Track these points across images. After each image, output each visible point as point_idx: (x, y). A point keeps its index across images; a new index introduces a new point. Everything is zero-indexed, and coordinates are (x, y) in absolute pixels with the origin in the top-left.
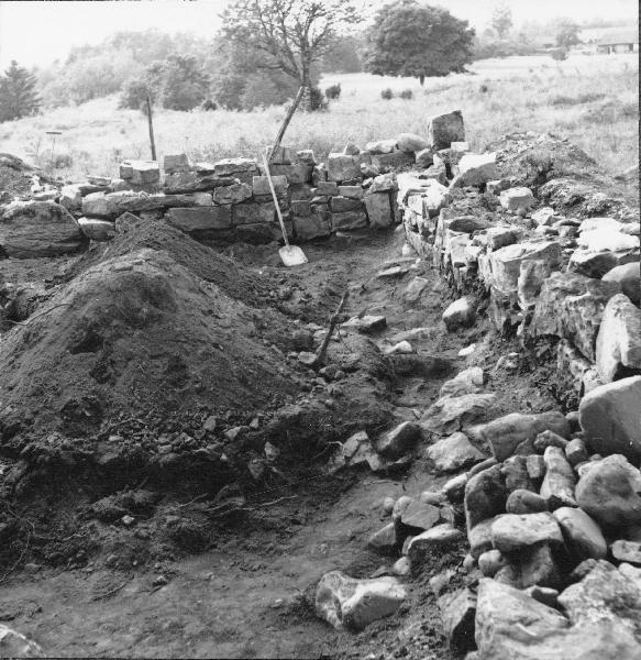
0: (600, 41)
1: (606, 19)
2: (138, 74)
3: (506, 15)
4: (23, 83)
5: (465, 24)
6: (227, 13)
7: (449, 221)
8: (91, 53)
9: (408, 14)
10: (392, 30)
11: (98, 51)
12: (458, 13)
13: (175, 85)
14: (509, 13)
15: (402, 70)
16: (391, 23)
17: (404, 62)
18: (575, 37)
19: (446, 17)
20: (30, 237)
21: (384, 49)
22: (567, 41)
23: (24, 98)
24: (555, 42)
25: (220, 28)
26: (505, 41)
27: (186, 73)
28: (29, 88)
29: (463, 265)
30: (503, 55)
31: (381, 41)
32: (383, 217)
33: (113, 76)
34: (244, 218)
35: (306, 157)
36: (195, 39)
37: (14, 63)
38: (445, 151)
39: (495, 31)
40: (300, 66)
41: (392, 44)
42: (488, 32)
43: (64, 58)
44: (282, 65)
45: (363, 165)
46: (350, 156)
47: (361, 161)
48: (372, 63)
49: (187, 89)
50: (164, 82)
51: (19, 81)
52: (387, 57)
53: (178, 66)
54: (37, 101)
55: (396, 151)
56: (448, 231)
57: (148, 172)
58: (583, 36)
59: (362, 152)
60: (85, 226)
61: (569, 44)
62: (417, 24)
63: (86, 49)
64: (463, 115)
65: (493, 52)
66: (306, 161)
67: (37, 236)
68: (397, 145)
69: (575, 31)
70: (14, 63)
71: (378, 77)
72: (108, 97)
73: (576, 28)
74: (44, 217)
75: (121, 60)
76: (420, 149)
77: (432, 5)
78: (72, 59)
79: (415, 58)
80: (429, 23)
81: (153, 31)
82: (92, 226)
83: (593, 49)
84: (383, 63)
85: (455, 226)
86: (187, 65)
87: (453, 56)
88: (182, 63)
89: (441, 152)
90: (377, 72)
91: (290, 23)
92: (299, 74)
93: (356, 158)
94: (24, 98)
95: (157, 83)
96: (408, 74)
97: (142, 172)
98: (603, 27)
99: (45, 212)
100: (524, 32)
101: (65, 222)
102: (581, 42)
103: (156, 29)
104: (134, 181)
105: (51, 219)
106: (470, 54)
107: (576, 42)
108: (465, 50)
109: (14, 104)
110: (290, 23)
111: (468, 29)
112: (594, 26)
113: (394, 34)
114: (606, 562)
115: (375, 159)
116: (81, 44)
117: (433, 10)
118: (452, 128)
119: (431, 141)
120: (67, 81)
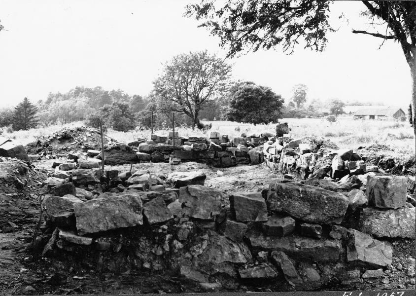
0: (355, 113)
1: (360, 101)
2: (96, 113)
3: (302, 95)
4: (30, 111)
5: (280, 97)
6: (157, 82)
7: (285, 153)
8: (60, 98)
9: (248, 90)
10: (240, 97)
11: (66, 98)
12: (276, 91)
13: (116, 119)
14: (305, 94)
15: (244, 120)
16: (240, 94)
17: (245, 115)
18: (342, 110)
19: (269, 92)
20: (116, 158)
21: (235, 107)
22: (337, 111)
23: (30, 119)
24: (329, 112)
25: (153, 89)
26: (301, 109)
27: (123, 112)
28: (33, 113)
29: (291, 165)
30: (299, 117)
31: (233, 103)
32: (256, 160)
33: (76, 112)
34: (202, 156)
35: (225, 137)
36: (123, 95)
37: (26, 99)
38: (281, 137)
39: (295, 104)
40: (194, 112)
41: (239, 104)
42: (291, 104)
43: (45, 100)
44: (184, 110)
45: (248, 141)
46: (242, 138)
47: (247, 140)
48: (228, 114)
49: (122, 121)
50: (110, 117)
51: (28, 109)
52: (237, 112)
53: (119, 108)
54: (37, 121)
55: (261, 137)
56: (285, 156)
57: (163, 137)
58: (346, 109)
59: (247, 136)
60: (139, 155)
61: (338, 113)
62: (254, 95)
63: (59, 95)
64: (288, 124)
65: (293, 115)
66: (225, 138)
67: (119, 158)
68: (261, 135)
69: (342, 106)
70: (26, 99)
71: (230, 122)
72: (72, 123)
73: (342, 105)
74: (123, 150)
75: (81, 102)
76: (270, 137)
77: (262, 85)
78: (49, 101)
79: (251, 113)
80: (260, 95)
81: (98, 89)
82: (142, 155)
83: (352, 117)
84: (234, 114)
85: (287, 154)
86: (123, 108)
87: (272, 113)
88: (121, 107)
89: (279, 138)
90: (231, 120)
91: (190, 90)
92: (193, 116)
93: (245, 139)
94: (30, 119)
95: (107, 116)
96: (247, 122)
97: (160, 137)
98: (358, 105)
99: (124, 149)
100: (312, 105)
101: (131, 153)
102: (345, 113)
103: (100, 88)
104: (157, 141)
105: (126, 151)
106: (281, 113)
107: (341, 113)
108: (279, 110)
109: (24, 122)
110: (190, 90)
111: (280, 100)
112: (353, 105)
113: (241, 100)
114: (313, 17)
115: (252, 139)
116: (55, 92)
117: (262, 88)
118: (284, 129)
119: (275, 134)
120: (48, 112)
